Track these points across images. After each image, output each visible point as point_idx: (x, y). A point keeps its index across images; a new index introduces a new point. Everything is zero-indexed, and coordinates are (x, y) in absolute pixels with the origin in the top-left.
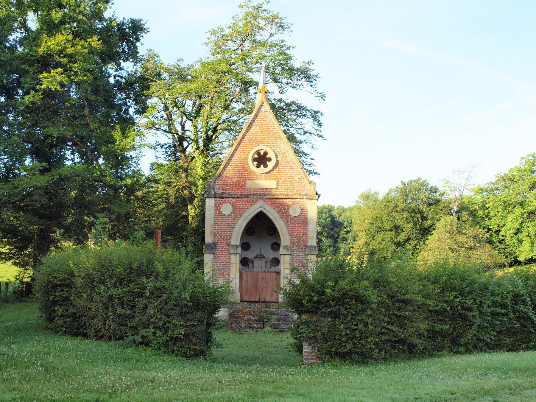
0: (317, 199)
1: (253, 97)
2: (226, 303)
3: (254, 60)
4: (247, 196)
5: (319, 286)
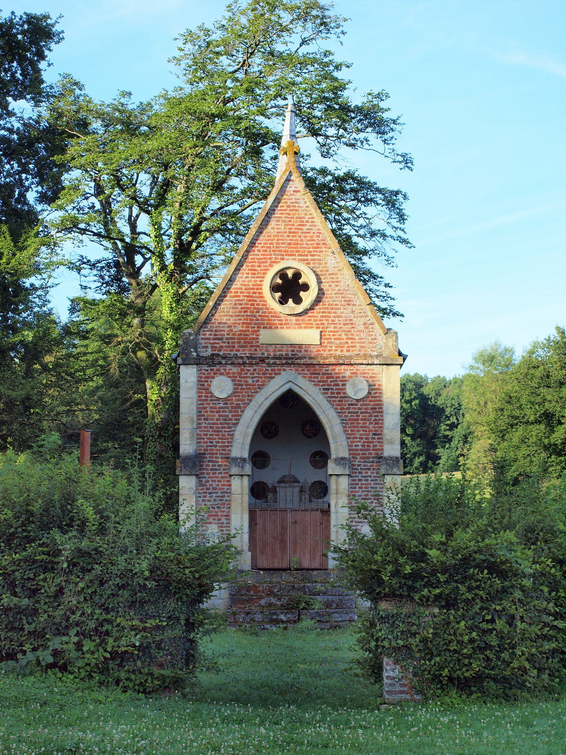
1: (270, 167)
2: (223, 575)
3: (272, 92)
5: (415, 543)
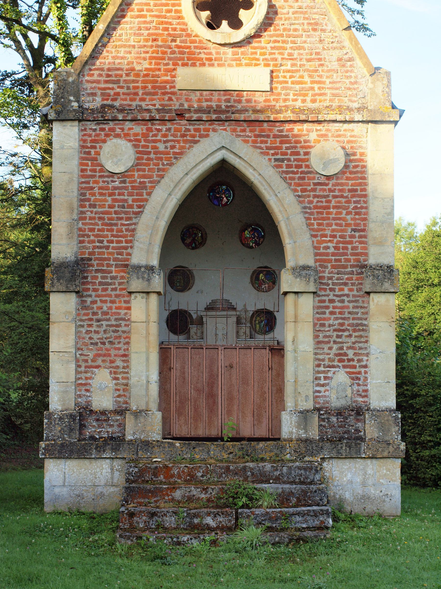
0: (396, 123)
4: (180, 115)
